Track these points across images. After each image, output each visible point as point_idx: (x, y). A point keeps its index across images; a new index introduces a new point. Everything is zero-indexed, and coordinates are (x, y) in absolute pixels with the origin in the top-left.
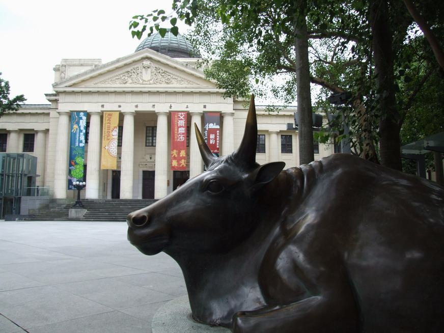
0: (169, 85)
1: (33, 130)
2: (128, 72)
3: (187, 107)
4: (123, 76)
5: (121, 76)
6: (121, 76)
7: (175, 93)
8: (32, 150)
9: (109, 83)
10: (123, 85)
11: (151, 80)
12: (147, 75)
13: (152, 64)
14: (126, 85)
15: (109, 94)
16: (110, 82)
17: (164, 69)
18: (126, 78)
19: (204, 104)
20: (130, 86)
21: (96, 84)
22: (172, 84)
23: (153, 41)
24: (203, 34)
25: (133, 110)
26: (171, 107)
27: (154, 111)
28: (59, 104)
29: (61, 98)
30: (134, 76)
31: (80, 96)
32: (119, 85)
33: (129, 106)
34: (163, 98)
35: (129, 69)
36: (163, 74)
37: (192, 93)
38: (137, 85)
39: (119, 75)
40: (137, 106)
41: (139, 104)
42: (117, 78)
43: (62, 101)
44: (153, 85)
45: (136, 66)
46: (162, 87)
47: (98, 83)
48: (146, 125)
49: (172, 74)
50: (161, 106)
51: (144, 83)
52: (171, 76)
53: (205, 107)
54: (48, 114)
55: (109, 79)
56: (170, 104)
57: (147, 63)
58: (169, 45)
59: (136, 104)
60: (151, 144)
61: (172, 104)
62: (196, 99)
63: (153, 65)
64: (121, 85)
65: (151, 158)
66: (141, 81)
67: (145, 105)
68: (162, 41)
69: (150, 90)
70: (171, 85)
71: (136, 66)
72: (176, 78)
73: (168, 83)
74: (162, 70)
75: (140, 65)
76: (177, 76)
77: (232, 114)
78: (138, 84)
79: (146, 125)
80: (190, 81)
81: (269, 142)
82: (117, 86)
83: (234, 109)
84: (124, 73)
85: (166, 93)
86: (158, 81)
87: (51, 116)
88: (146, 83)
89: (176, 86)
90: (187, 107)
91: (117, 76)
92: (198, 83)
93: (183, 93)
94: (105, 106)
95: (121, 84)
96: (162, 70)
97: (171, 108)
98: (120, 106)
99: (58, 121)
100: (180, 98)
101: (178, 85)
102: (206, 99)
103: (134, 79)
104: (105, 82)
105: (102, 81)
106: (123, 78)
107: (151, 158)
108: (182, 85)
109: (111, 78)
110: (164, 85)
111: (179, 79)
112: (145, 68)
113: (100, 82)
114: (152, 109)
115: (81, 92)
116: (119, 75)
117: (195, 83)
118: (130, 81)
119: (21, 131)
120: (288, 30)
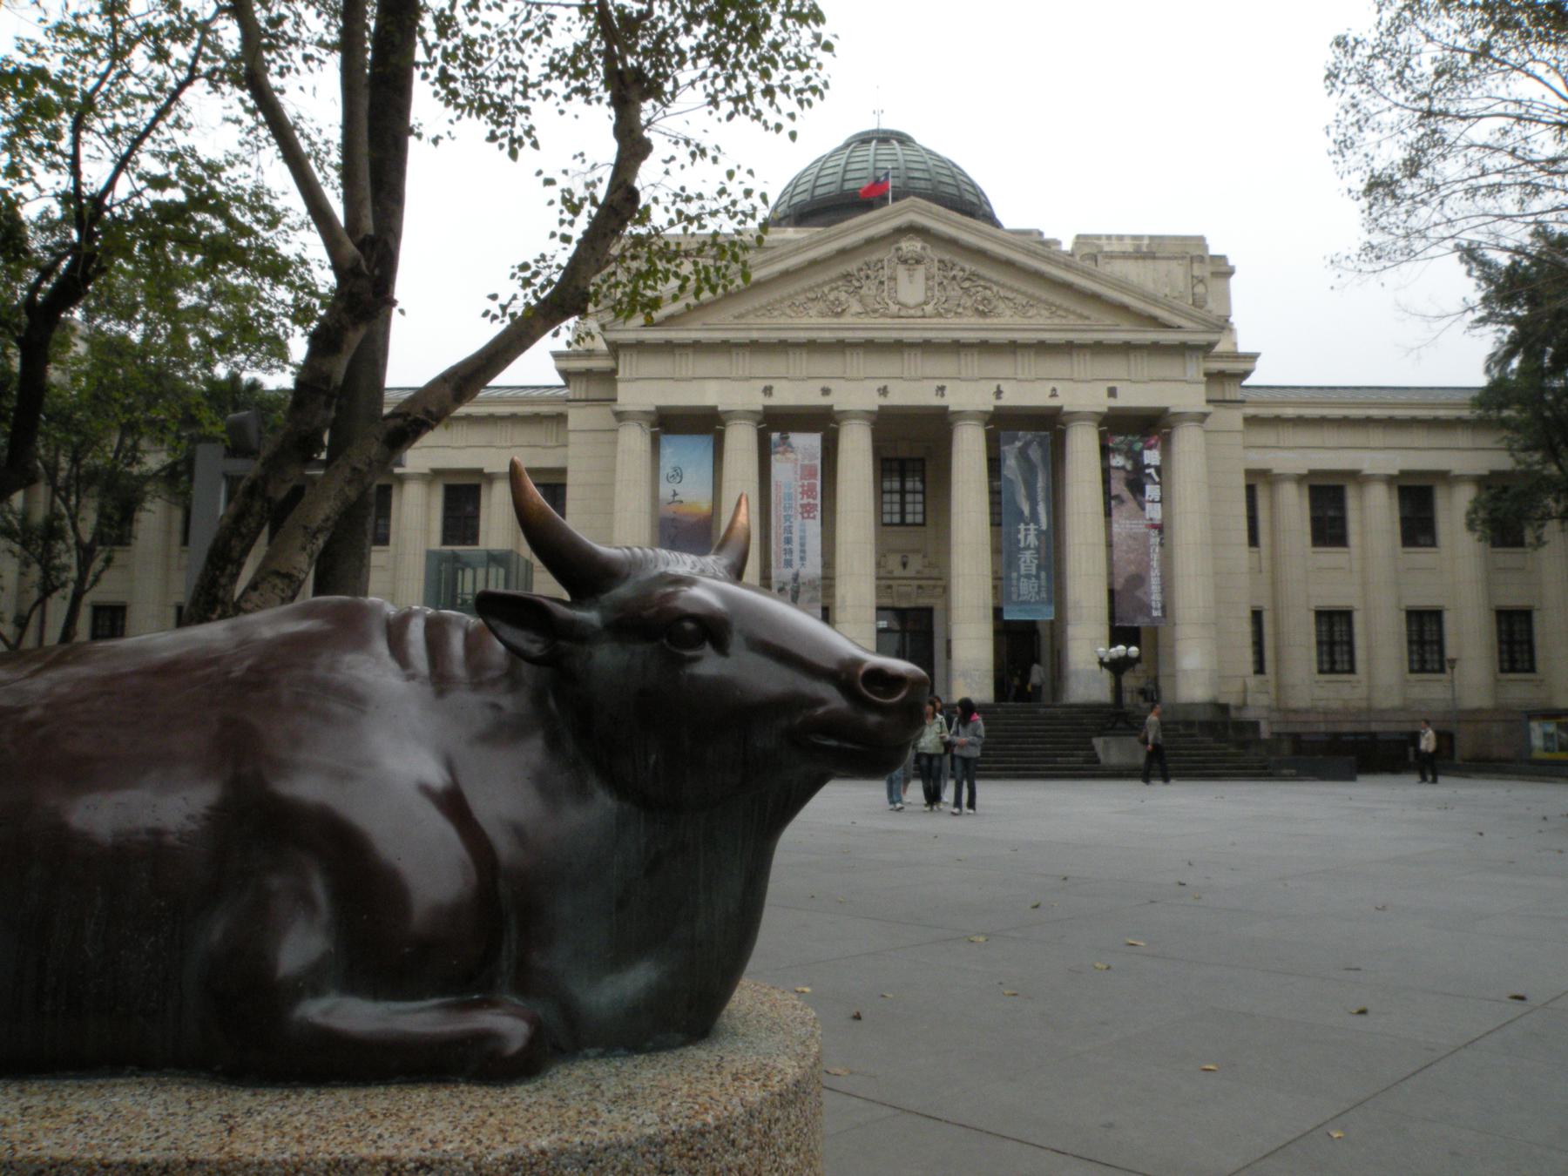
0: (988, 321)
1: (479, 472)
2: (847, 277)
3: (1054, 394)
4: (832, 289)
5: (826, 289)
6: (826, 289)
7: (1013, 348)
8: (472, 536)
9: (784, 313)
10: (835, 320)
11: (926, 303)
12: (911, 288)
13: (929, 251)
14: (842, 320)
15: (729, 352)
16: (788, 311)
17: (970, 267)
18: (843, 296)
19: (1111, 384)
20: (855, 323)
21: (741, 316)
22: (999, 315)
23: (845, 171)
24: (1423, 172)
25: (873, 402)
26: (999, 393)
27: (946, 408)
28: (621, 387)
29: (627, 367)
30: (869, 289)
31: (691, 357)
32: (821, 320)
33: (857, 391)
34: (973, 364)
35: (852, 267)
36: (966, 284)
37: (1069, 348)
38: (881, 320)
39: (819, 286)
40: (884, 391)
41: (891, 384)
42: (811, 295)
43: (627, 375)
44: (935, 320)
45: (874, 257)
46: (966, 326)
47: (748, 313)
48: (912, 452)
49: (996, 283)
50: (970, 392)
51: (903, 313)
52: (995, 289)
53: (1112, 392)
54: (561, 418)
55: (782, 301)
56: (994, 384)
57: (911, 246)
58: (309, 155)
59: (881, 384)
60: (897, 519)
61: (1001, 382)
62: (1085, 366)
63: (934, 254)
64: (827, 320)
65: (904, 565)
66: (894, 308)
67: (913, 389)
68: (848, 176)
69: (755, 335)
70: (995, 321)
71: (874, 257)
72: (1011, 295)
73: (983, 314)
74: (963, 270)
75: (886, 254)
76: (1011, 289)
77: (1202, 417)
78: (884, 315)
79: (912, 452)
80: (1059, 307)
81: (1362, 509)
82: (810, 322)
83: (1209, 401)
84: (832, 281)
85: (985, 347)
86: (951, 305)
87: (571, 424)
88: (912, 312)
89: (1008, 322)
90: (1054, 394)
91: (811, 289)
92: (1086, 313)
93: (1043, 348)
94: (775, 391)
95: (823, 315)
96: (963, 270)
97: (1054, 390)
98: (826, 392)
99: (615, 443)
100: (1028, 366)
101: (1019, 321)
102: (1115, 368)
103: (870, 301)
104: (769, 309)
105: (762, 307)
106: (831, 297)
107: (904, 565)
108: (1032, 321)
109: (790, 296)
110: (973, 320)
111: (1021, 300)
112: (905, 262)
113: (756, 309)
114: (936, 401)
115: (697, 347)
116: (819, 286)
117: (1074, 313)
118: (856, 307)
119: (437, 474)
120: (629, 79)
